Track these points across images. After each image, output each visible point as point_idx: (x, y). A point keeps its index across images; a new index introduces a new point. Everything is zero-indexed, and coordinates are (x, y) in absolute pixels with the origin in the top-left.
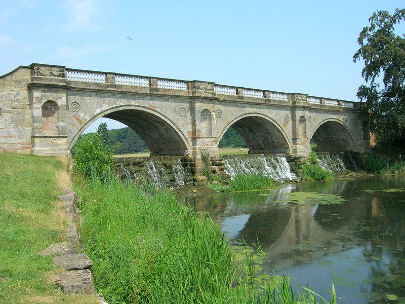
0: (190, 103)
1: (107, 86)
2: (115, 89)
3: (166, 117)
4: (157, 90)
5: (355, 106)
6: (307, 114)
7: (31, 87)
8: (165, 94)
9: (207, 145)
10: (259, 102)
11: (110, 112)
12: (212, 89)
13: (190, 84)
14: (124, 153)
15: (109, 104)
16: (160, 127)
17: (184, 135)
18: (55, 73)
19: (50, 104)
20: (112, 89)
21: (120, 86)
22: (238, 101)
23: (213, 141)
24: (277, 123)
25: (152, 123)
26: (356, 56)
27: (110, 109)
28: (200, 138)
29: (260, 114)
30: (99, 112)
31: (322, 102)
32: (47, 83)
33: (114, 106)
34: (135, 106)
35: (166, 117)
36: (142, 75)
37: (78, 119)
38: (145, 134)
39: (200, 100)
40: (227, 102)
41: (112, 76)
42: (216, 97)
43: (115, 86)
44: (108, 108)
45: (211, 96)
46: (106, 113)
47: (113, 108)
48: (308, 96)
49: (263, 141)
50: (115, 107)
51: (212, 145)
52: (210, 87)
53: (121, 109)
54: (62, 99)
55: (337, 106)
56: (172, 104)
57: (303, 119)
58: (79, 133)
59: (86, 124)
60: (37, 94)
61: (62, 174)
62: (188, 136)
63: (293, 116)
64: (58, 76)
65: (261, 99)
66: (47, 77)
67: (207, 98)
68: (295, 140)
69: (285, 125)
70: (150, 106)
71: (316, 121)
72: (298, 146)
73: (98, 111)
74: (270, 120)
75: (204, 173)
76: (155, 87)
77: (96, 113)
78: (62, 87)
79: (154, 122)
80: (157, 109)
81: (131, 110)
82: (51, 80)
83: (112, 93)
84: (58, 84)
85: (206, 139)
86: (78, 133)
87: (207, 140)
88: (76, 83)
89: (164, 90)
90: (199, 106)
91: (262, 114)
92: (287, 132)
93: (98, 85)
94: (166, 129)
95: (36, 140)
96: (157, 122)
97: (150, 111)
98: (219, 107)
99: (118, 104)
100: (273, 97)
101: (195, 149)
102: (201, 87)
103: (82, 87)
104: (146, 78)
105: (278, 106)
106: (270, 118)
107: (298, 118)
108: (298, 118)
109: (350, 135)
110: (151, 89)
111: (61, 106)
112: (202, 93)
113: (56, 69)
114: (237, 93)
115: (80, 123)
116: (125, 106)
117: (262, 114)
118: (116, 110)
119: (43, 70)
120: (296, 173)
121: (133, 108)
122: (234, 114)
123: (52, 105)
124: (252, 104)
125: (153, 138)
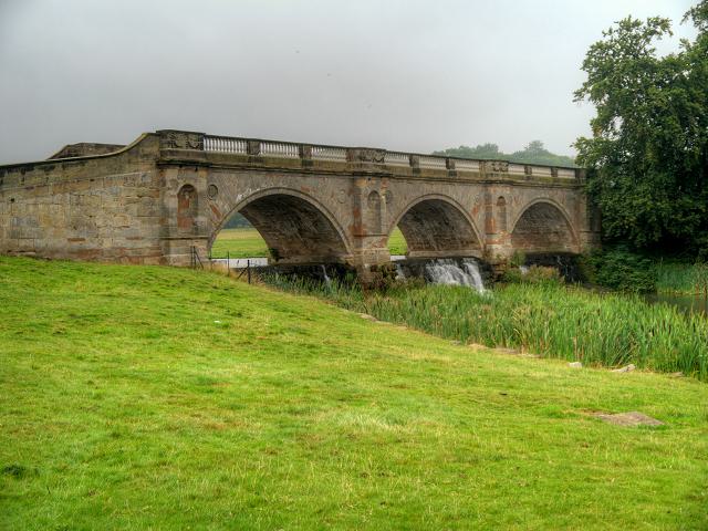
0: (353, 181)
1: (250, 160)
3: (322, 205)
4: (311, 163)
5: (349, 158)
6: (505, 191)
7: (162, 165)
12: (382, 160)
15: (252, 187)
17: (343, 232)
18: (193, 143)
20: (258, 165)
22: (529, 182)
26: (579, 94)
28: (366, 236)
32: (185, 158)
36: (317, 143)
43: (260, 160)
44: (251, 193)
48: (202, 136)
53: (267, 193)
54: (201, 181)
56: (331, 182)
57: (501, 201)
60: (171, 174)
62: (348, 233)
63: (488, 199)
66: (184, 150)
67: (376, 175)
68: (489, 232)
69: (475, 211)
71: (519, 201)
72: (494, 246)
74: (454, 204)
75: (379, 304)
76: (308, 159)
79: (297, 211)
80: (311, 193)
83: (257, 170)
87: (375, 239)
92: (478, 221)
93: (236, 157)
95: (172, 243)
97: (301, 196)
98: (391, 184)
99: (264, 186)
101: (359, 253)
104: (297, 144)
105: (465, 180)
107: (495, 199)
108: (495, 199)
109: (568, 225)
110: (305, 163)
111: (201, 193)
112: (371, 168)
113: (194, 137)
115: (218, 216)
118: (261, 195)
119: (181, 142)
121: (281, 191)
122: (410, 195)
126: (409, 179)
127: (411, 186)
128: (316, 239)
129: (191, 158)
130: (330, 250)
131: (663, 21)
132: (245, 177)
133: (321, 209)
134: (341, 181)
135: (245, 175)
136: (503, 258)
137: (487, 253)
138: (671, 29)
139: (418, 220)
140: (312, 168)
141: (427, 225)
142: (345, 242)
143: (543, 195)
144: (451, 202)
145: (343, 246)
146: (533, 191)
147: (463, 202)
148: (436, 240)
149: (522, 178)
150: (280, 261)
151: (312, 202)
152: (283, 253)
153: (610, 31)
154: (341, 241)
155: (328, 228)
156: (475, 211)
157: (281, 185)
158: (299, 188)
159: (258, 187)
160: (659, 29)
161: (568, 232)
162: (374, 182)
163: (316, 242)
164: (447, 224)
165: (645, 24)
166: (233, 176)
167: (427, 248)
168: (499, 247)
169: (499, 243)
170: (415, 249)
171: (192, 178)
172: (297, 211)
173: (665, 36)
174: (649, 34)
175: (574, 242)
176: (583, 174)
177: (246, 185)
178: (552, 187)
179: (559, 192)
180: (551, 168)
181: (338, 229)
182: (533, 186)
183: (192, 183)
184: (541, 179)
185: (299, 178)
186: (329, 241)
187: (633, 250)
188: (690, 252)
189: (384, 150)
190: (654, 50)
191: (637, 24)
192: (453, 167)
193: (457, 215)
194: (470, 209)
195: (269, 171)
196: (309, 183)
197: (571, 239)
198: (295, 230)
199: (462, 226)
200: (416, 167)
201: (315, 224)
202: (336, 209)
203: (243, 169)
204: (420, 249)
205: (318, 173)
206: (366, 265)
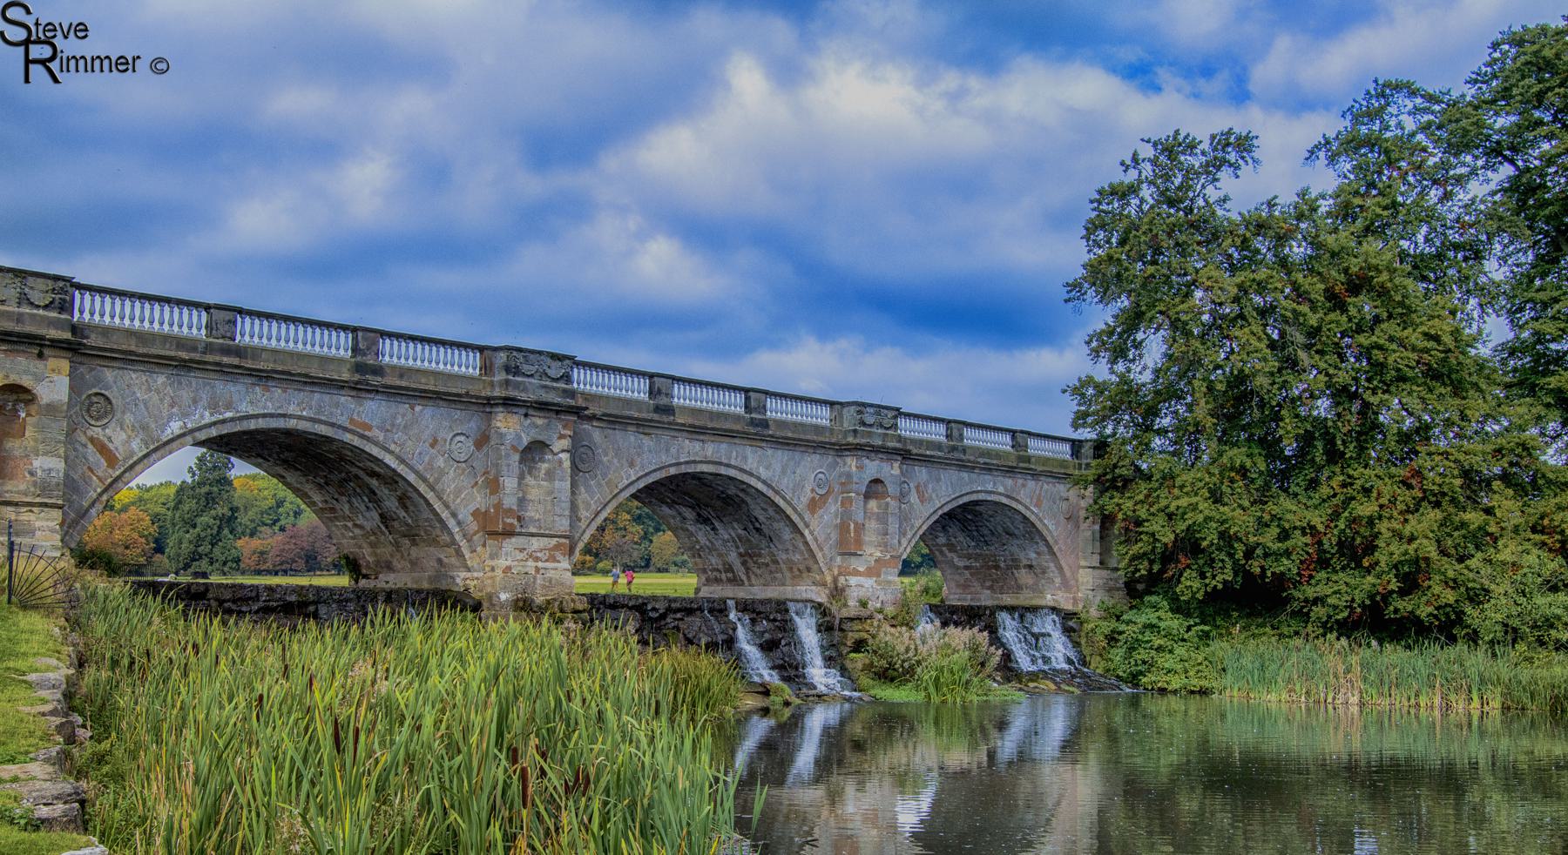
1: (209, 348)
2: (236, 361)
4: (378, 370)
5: (487, 368)
8: (404, 384)
9: (537, 559)
10: (728, 425)
11: (214, 432)
12: (567, 378)
13: (360, 334)
14: (297, 573)
15: (213, 407)
16: (383, 491)
18: (36, 297)
19: (15, 397)
20: (226, 360)
21: (256, 352)
23: (557, 547)
24: (784, 499)
25: (357, 477)
27: (214, 424)
29: (728, 466)
30: (177, 432)
31: (956, 433)
33: (229, 415)
34: (300, 418)
35: (402, 461)
37: (103, 449)
38: (333, 510)
39: (523, 411)
40: (617, 419)
41: (228, 315)
42: (581, 402)
43: (239, 352)
44: (208, 419)
45: (558, 400)
46: (202, 436)
47: (223, 422)
48: (898, 413)
49: (741, 555)
50: (232, 420)
51: (553, 559)
52: (556, 370)
53: (252, 425)
55: (943, 439)
56: (429, 418)
58: (105, 498)
59: (132, 467)
61: (610, 637)
64: (46, 307)
65: (737, 418)
69: (814, 505)
70: (352, 421)
73: (175, 427)
74: (760, 486)
77: (168, 434)
78: (56, 344)
79: (361, 474)
81: (288, 433)
82: (19, 318)
83: (221, 370)
84: (42, 331)
85: (534, 540)
86: (100, 495)
88: (106, 331)
89: (403, 372)
90: (509, 426)
91: (735, 467)
94: (403, 500)
96: (373, 474)
97: (347, 437)
99: (245, 408)
100: (972, 438)
102: (525, 368)
103: (124, 347)
106: (764, 482)
110: (360, 368)
113: (41, 284)
114: (652, 393)
116: (264, 416)
117: (735, 467)
120: (843, 671)
121: (292, 424)
123: (17, 401)
124: (703, 427)
125: (361, 527)
126: (642, 425)
127: (646, 441)
128: (413, 537)
129: (29, 328)
130: (440, 561)
131: (1239, 138)
132: (191, 387)
133: (401, 469)
134: (458, 414)
135: (194, 380)
136: (874, 605)
137: (838, 592)
138: (65, 18)
139: (706, 521)
140: (374, 380)
141: (724, 533)
142: (463, 543)
143: (990, 487)
144: (753, 482)
145: (459, 554)
146: (965, 475)
147: (785, 484)
148: (744, 563)
149: (938, 446)
150: (363, 583)
151: (375, 451)
152: (368, 567)
153: (1135, 159)
154: (454, 542)
155: (426, 514)
156: (814, 505)
157: (292, 409)
158: (343, 420)
159: (229, 407)
160: (1232, 157)
161: (1052, 565)
162: (540, 422)
163: (414, 543)
164: (758, 530)
165: (1205, 146)
166: (161, 379)
167: (729, 580)
168: (869, 582)
169: (870, 573)
170: (708, 581)
171: (26, 372)
172: (361, 474)
173: (1246, 170)
174: (1214, 166)
175: (1066, 585)
176: (1087, 450)
177: (195, 401)
178: (1010, 471)
179: (1031, 484)
180: (1013, 433)
181: (445, 515)
182: (962, 466)
183: (26, 381)
184: (1046, 461)
185: (345, 399)
186: (434, 542)
187: (1178, 608)
188: (1294, 614)
189: (571, 358)
190: (1225, 200)
191: (1192, 147)
192: (961, 437)
193: (771, 511)
194: (802, 502)
195: (263, 377)
196: (372, 410)
197: (1058, 580)
198: (377, 517)
199: (787, 534)
200: (663, 401)
201: (403, 500)
202: (442, 473)
203: (185, 366)
204: (718, 581)
205: (395, 393)
206: (503, 597)
